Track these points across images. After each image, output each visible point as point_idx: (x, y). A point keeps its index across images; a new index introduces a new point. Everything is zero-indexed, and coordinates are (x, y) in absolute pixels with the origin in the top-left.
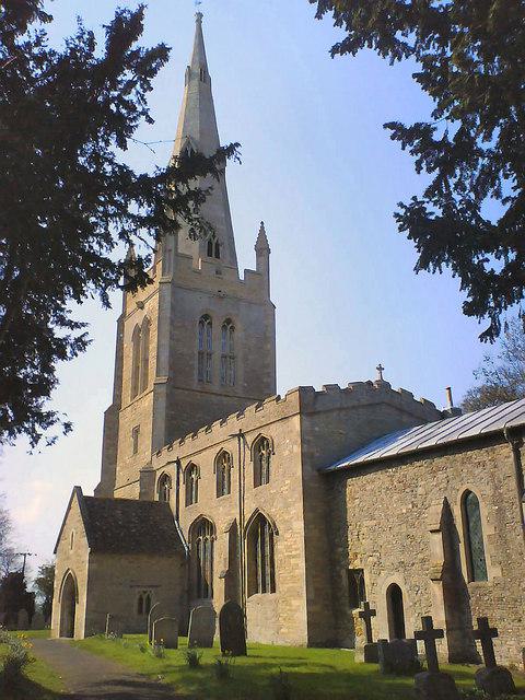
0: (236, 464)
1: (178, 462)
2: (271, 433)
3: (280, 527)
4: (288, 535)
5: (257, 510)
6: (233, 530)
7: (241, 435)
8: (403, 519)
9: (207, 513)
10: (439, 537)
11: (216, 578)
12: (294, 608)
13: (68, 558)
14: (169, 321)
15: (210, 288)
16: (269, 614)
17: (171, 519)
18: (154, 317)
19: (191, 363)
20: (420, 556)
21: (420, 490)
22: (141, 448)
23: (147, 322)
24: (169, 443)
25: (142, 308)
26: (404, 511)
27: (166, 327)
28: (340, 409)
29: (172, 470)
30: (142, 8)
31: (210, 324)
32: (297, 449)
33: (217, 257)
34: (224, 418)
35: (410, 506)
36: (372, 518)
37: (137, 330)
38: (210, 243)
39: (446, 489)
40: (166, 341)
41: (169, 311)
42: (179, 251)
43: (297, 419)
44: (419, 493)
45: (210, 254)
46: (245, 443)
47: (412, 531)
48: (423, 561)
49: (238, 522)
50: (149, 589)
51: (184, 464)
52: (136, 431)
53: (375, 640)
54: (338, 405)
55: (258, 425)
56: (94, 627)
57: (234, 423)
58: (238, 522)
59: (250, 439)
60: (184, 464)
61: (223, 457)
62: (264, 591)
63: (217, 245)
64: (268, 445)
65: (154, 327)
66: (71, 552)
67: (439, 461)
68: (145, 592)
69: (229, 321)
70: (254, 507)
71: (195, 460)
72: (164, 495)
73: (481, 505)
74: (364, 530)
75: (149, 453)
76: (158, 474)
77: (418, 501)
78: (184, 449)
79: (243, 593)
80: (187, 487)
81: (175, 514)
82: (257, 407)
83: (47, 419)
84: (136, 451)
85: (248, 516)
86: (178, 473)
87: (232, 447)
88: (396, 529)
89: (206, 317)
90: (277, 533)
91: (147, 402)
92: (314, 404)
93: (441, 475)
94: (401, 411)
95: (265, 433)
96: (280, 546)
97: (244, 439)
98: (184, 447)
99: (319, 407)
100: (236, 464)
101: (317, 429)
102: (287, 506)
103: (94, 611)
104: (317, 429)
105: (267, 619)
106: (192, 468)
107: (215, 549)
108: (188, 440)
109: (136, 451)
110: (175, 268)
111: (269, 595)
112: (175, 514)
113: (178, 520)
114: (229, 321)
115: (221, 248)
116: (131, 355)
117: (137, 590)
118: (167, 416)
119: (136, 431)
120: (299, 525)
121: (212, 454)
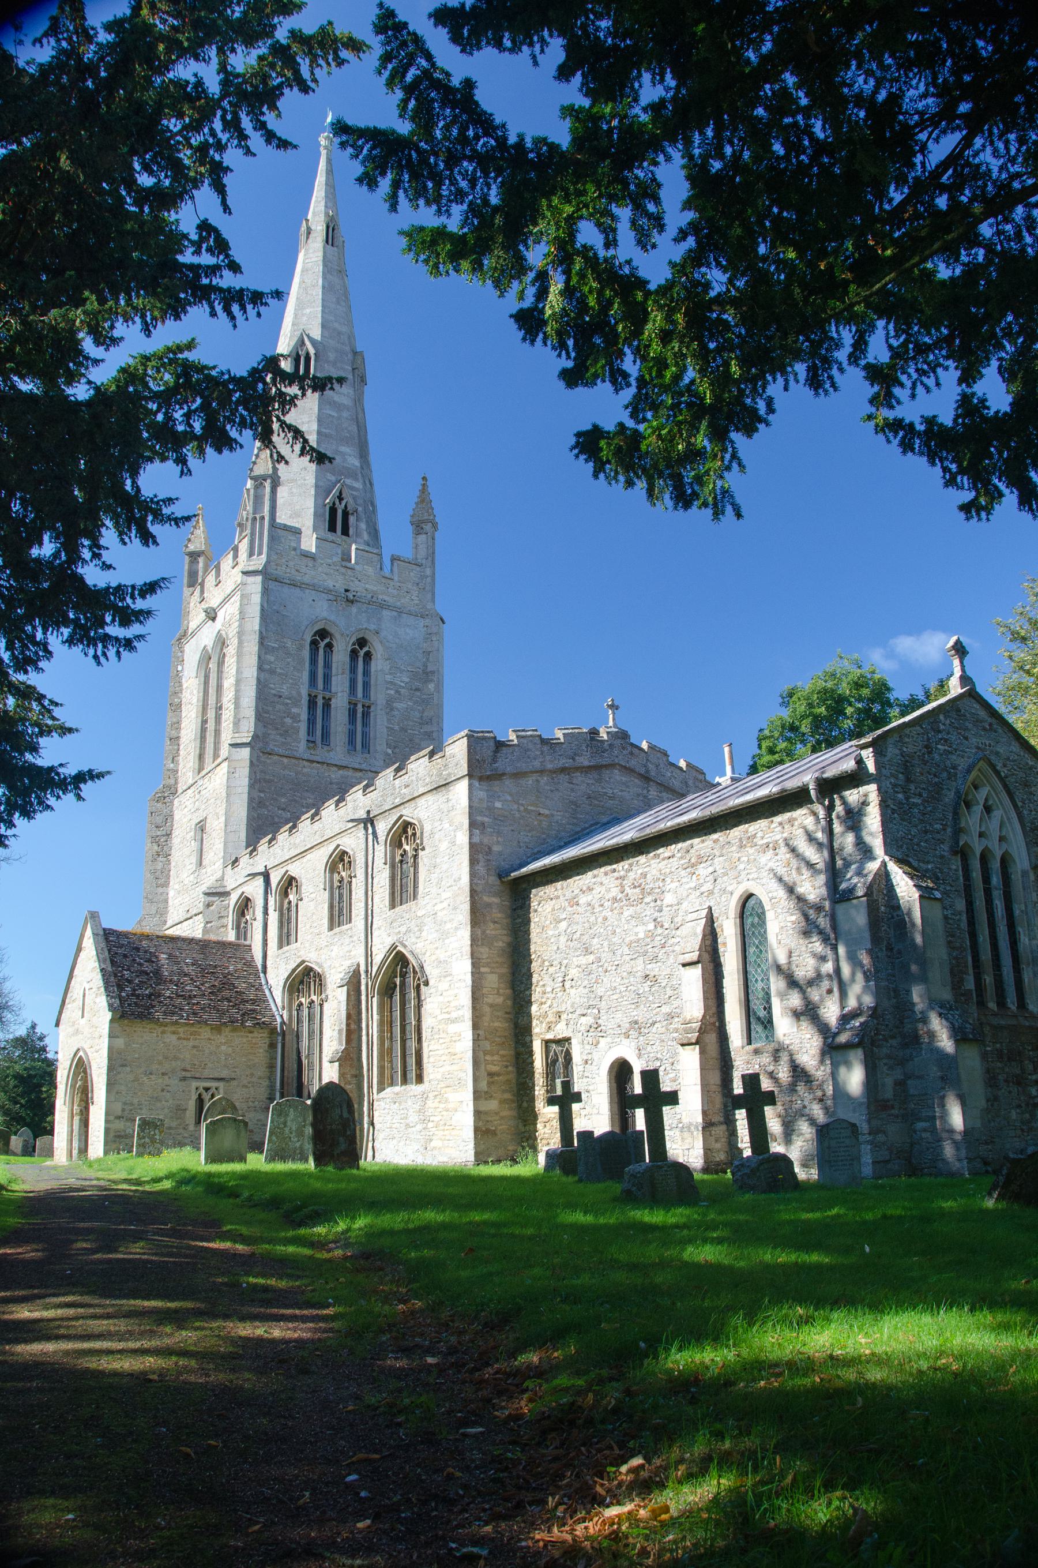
0: (360, 873)
1: (266, 876)
2: (421, 813)
3: (432, 972)
4: (443, 985)
5: (394, 947)
6: (353, 983)
7: (369, 821)
8: (639, 949)
9: (313, 958)
10: (697, 972)
11: (326, 1064)
12: (450, 1106)
13: (77, 1032)
14: (257, 637)
15: (330, 583)
16: (413, 1118)
17: (254, 973)
18: (232, 632)
19: (294, 710)
20: (665, 1009)
21: (669, 899)
22: (209, 857)
23: (221, 642)
24: (252, 844)
25: (214, 619)
26: (641, 935)
27: (252, 647)
28: (541, 772)
29: (255, 889)
30: (255, 155)
31: (329, 646)
32: (463, 839)
33: (345, 532)
34: (341, 793)
35: (651, 926)
36: (587, 951)
37: (206, 658)
38: (333, 510)
39: (711, 893)
40: (251, 672)
41: (257, 620)
42: (278, 521)
43: (463, 786)
44: (666, 902)
45: (332, 528)
46: (374, 834)
47: (654, 969)
48: (670, 1016)
49: (362, 968)
50: (213, 1084)
51: (275, 879)
52: (201, 827)
53: (324, 1083)
54: (537, 764)
55: (397, 801)
56: (115, 1140)
57: (358, 802)
58: (362, 968)
59: (383, 827)
60: (275, 879)
61: (340, 860)
62: (405, 1081)
63: (346, 514)
64: (414, 834)
65: (231, 651)
66: (83, 1021)
67: (699, 845)
68: (207, 1089)
69: (362, 642)
70: (388, 942)
71: (294, 869)
72: (241, 929)
73: (770, 916)
74: (573, 972)
75: (219, 864)
76: (234, 897)
77: (665, 918)
78: (269, 855)
79: (370, 1086)
80: (281, 915)
81: (259, 961)
82: (397, 770)
83: (579, 1094)
84: (200, 863)
85: (378, 959)
86: (266, 893)
87: (354, 842)
88: (627, 967)
89: (323, 633)
90: (427, 984)
91: (218, 779)
92: (494, 760)
93: (703, 870)
94: (646, 778)
95: (408, 813)
96: (430, 1006)
97: (372, 824)
98: (276, 848)
99: (501, 765)
100: (360, 873)
101: (498, 805)
102: (444, 935)
103: (119, 1118)
104: (498, 805)
105: (408, 1126)
106: (290, 883)
107: (325, 1017)
108: (283, 837)
109: (200, 863)
110: (269, 548)
111: (413, 1088)
112: (259, 961)
113: (265, 972)
114: (362, 642)
115: (352, 519)
116: (195, 701)
117: (195, 1084)
118: (251, 800)
119: (201, 827)
120: (463, 968)
121: (321, 857)
